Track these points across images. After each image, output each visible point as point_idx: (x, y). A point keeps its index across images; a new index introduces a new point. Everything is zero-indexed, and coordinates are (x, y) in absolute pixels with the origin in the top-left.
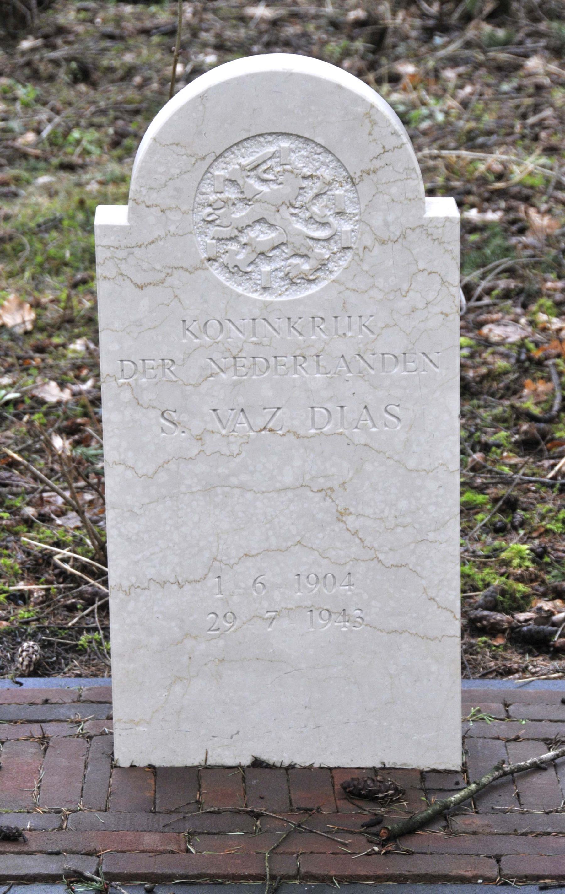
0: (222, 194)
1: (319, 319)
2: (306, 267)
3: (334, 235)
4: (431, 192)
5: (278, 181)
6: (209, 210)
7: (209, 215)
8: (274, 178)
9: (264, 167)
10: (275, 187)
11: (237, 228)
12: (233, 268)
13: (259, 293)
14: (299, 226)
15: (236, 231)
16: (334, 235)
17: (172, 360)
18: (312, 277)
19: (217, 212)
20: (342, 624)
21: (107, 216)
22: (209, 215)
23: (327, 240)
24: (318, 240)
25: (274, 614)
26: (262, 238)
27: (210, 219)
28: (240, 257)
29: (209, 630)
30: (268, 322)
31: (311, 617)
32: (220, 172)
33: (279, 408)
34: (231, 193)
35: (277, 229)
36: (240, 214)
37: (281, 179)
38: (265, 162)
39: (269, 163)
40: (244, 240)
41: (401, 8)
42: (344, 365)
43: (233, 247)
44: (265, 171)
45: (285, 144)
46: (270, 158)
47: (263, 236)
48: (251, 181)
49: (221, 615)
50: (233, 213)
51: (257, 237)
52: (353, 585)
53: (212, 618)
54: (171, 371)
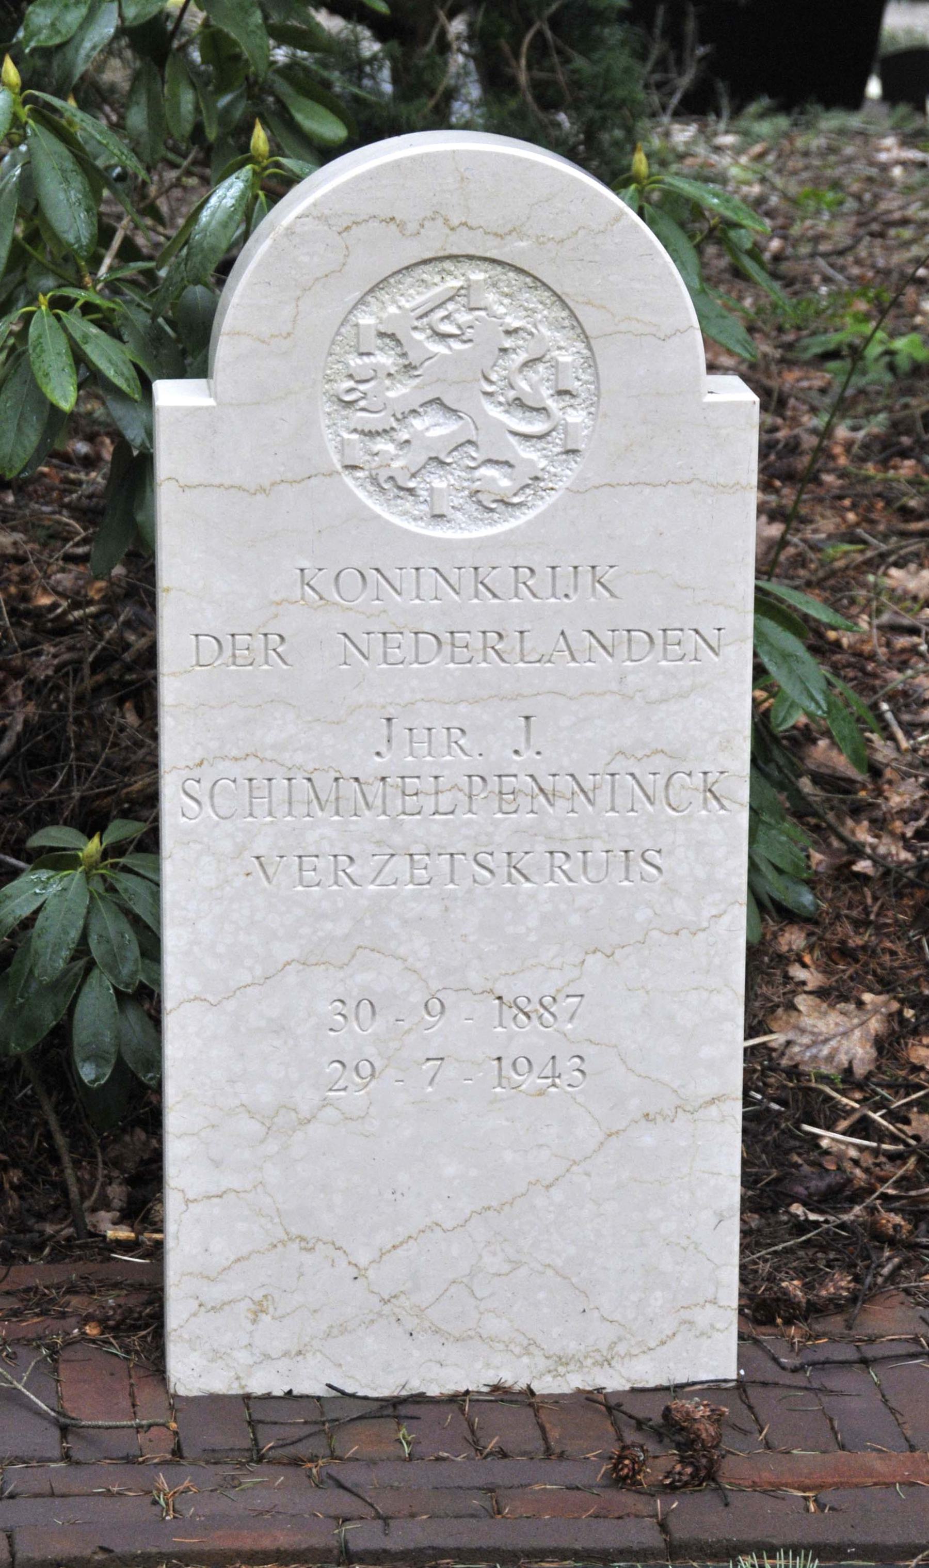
0: (372, 358)
1: (527, 570)
2: (505, 483)
3: (553, 430)
4: (712, 368)
5: (464, 338)
6: (351, 384)
7: (350, 390)
8: (458, 332)
9: (442, 313)
10: (457, 345)
11: (394, 415)
12: (386, 481)
13: (502, 408)
14: (495, 412)
15: (392, 419)
16: (553, 430)
17: (280, 636)
18: (516, 500)
19: (362, 387)
20: (549, 1081)
21: (169, 393)
22: (351, 390)
23: (540, 437)
24: (527, 437)
25: (579, 999)
26: (435, 433)
27: (348, 398)
28: (396, 464)
29: (330, 1090)
30: (441, 575)
31: (500, 1069)
32: (366, 320)
33: (393, 855)
34: (386, 360)
35: (461, 418)
36: (400, 392)
37: (469, 333)
38: (444, 303)
39: (451, 306)
40: (404, 436)
41: (896, 135)
42: (565, 648)
43: (383, 446)
44: (443, 319)
45: (478, 275)
46: (451, 299)
47: (434, 428)
48: (418, 336)
49: (351, 1065)
50: (388, 389)
51: (427, 429)
52: (559, 1077)
53: (336, 1069)
54: (278, 654)
